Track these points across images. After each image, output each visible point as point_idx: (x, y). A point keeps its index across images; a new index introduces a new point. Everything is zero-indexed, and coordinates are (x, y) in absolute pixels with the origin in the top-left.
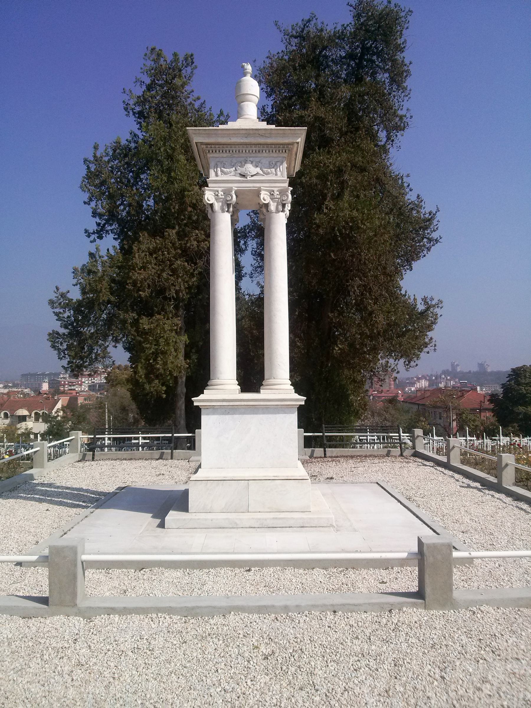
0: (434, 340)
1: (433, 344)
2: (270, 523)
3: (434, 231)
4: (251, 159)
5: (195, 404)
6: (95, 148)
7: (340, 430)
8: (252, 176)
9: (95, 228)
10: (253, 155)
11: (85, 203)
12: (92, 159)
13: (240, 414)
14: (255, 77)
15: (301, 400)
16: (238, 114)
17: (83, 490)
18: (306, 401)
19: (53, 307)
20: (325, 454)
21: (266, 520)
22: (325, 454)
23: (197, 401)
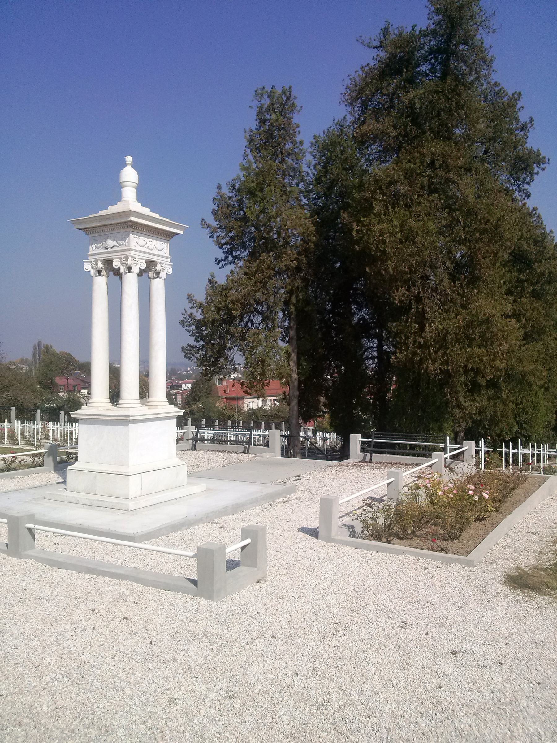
2: (95, 503)
4: (111, 235)
5: (73, 416)
6: (217, 188)
7: (387, 437)
8: (112, 248)
10: (111, 232)
11: (210, 237)
13: (98, 425)
14: (133, 166)
16: (117, 197)
19: (183, 326)
20: (371, 459)
22: (371, 459)
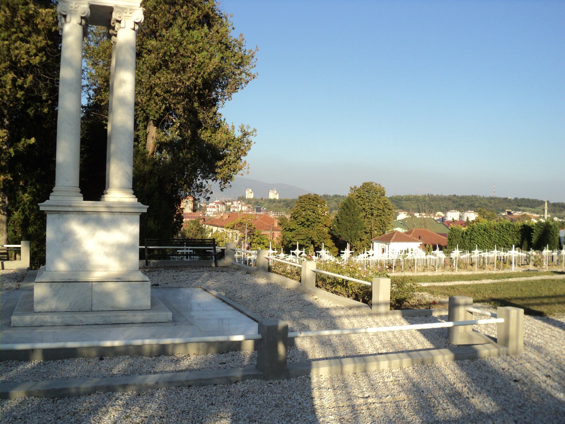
0: (247, 164)
1: (246, 167)
3: (252, 67)
14: (40, 8)
15: (144, 209)
17: (206, 91)
18: (148, 209)
21: (109, 317)
23: (43, 207)
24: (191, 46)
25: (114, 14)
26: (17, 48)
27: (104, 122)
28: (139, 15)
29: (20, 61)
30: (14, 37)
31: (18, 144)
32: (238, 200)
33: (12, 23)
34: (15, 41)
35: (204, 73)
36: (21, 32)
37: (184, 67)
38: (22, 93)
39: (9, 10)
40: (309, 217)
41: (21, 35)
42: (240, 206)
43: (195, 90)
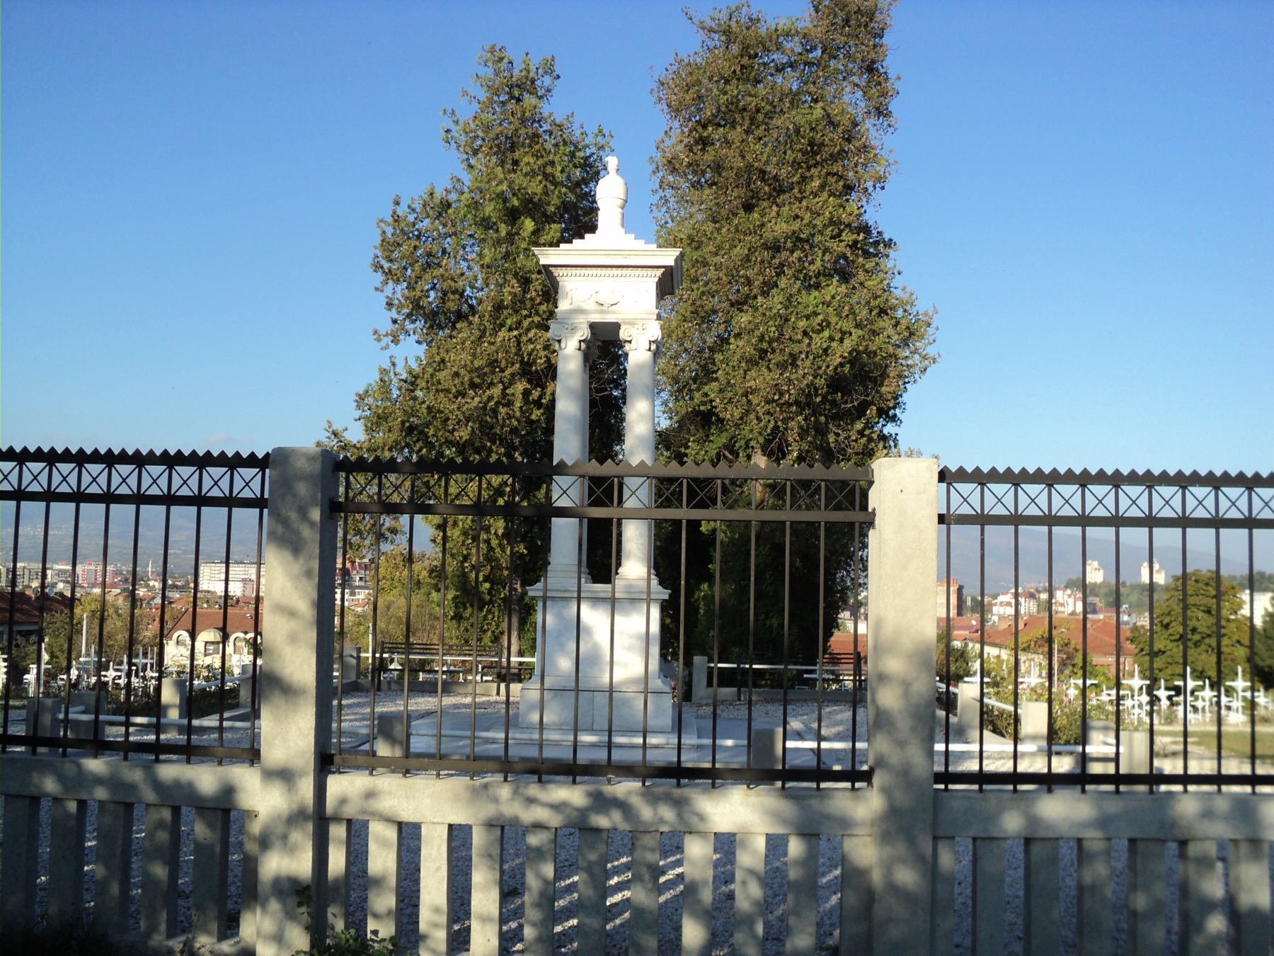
9: (389, 327)
11: (377, 289)
12: (390, 220)
24: (802, 324)
25: (621, 332)
26: (530, 340)
27: (683, 450)
28: (655, 331)
29: (534, 362)
30: (526, 323)
31: (537, 493)
32: (1066, 587)
33: (523, 302)
34: (528, 330)
35: (828, 367)
36: (537, 314)
37: (794, 360)
38: (539, 412)
39: (518, 281)
40: (1197, 624)
41: (537, 319)
42: (1071, 601)
43: (817, 395)
